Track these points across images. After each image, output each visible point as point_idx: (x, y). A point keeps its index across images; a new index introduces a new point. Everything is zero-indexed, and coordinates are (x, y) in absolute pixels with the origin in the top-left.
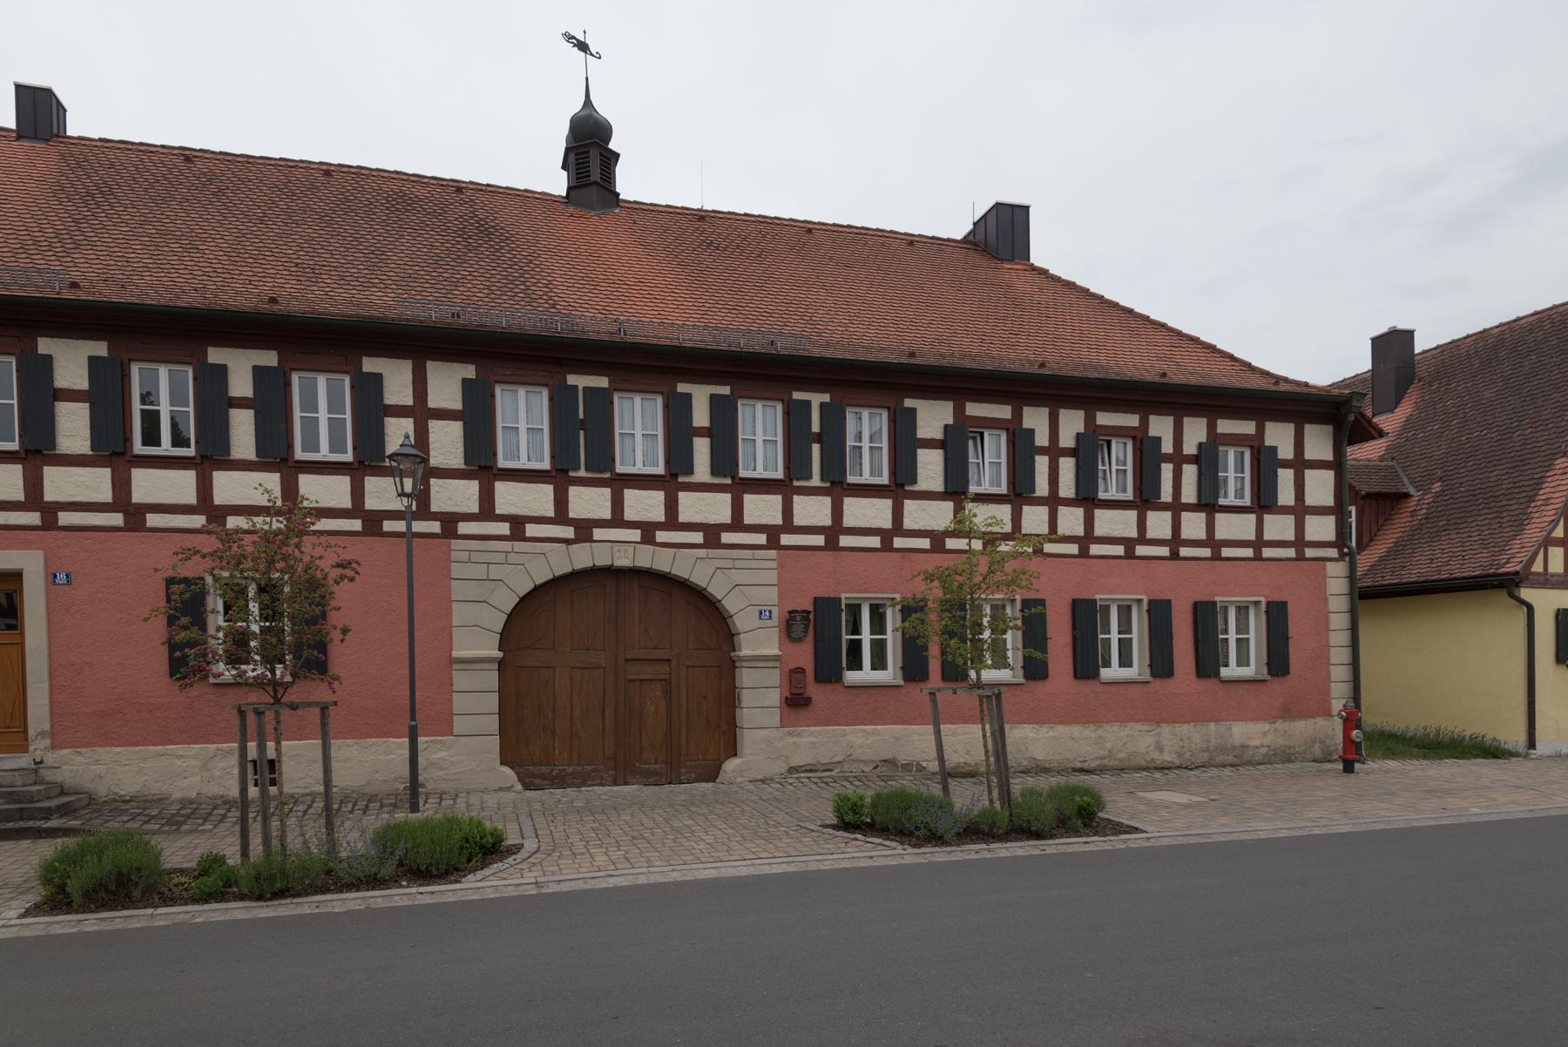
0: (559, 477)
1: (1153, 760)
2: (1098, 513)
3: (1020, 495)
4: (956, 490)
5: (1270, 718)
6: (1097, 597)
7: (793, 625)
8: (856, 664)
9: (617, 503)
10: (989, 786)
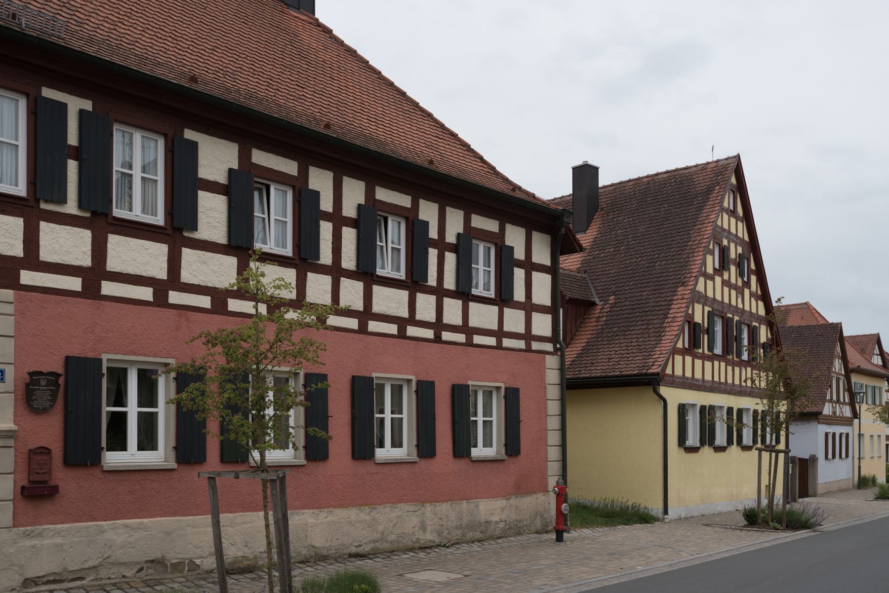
3: (304, 260)
5: (506, 496)
6: (374, 375)
8: (119, 443)
10: (271, 583)
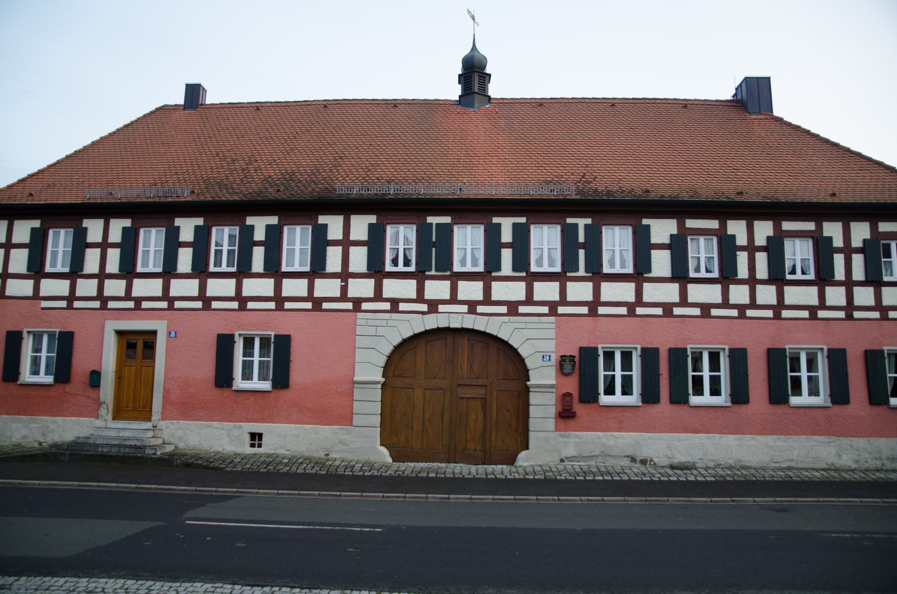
0: (420, 276)
1: (833, 464)
2: (690, 287)
3: (727, 278)
4: (680, 275)
7: (564, 364)
8: (699, 391)
9: (454, 290)
